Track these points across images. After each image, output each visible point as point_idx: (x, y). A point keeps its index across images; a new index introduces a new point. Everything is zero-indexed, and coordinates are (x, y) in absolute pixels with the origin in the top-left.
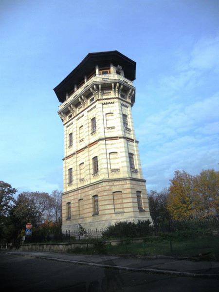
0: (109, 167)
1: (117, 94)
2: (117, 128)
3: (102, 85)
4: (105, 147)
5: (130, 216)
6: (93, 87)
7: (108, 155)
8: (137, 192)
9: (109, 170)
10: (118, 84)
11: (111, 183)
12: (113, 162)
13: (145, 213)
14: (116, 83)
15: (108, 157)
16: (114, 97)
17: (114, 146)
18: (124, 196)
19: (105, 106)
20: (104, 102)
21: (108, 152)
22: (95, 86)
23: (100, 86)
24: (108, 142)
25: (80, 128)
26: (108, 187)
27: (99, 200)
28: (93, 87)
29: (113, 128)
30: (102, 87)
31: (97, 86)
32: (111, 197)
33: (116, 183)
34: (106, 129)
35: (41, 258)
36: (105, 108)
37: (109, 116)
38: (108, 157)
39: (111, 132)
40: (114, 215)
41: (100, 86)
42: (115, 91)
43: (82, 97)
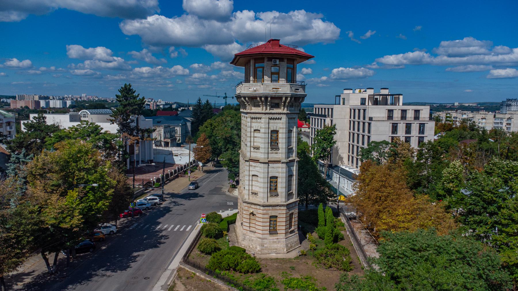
0: (250, 188)
1: (286, 109)
2: (262, 150)
4: (248, 169)
5: (259, 237)
7: (251, 177)
8: (271, 217)
9: (250, 191)
11: (249, 205)
12: (255, 184)
13: (278, 235)
14: (288, 97)
15: (251, 179)
17: (257, 169)
18: (257, 219)
19: (254, 120)
20: (271, 116)
21: (252, 173)
22: (263, 99)
24: (252, 163)
25: (255, 130)
26: (247, 208)
27: (278, 221)
28: (286, 98)
29: (258, 148)
30: (271, 99)
31: (266, 98)
32: (248, 217)
33: (253, 206)
34: (252, 148)
35: (17, 256)
36: (254, 122)
37: (257, 133)
38: (251, 179)
39: (256, 152)
40: (249, 232)
43: (247, 99)
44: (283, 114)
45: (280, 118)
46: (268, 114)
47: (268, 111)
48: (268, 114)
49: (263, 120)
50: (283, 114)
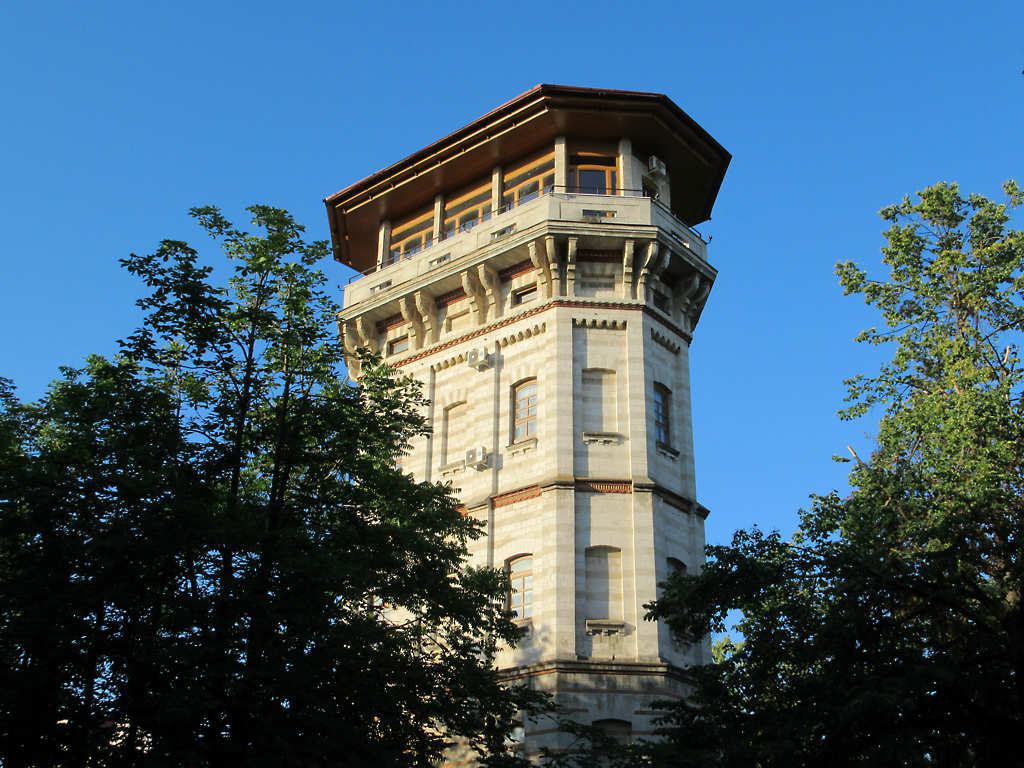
3: (581, 239)
6: (410, 298)
10: (652, 249)
16: (629, 300)
22: (549, 244)
23: (572, 246)
41: (572, 246)
42: (635, 275)
44: (630, 307)
45: (619, 323)
46: (569, 304)
47: (570, 297)
48: (569, 304)
49: (551, 332)
50: (630, 307)
